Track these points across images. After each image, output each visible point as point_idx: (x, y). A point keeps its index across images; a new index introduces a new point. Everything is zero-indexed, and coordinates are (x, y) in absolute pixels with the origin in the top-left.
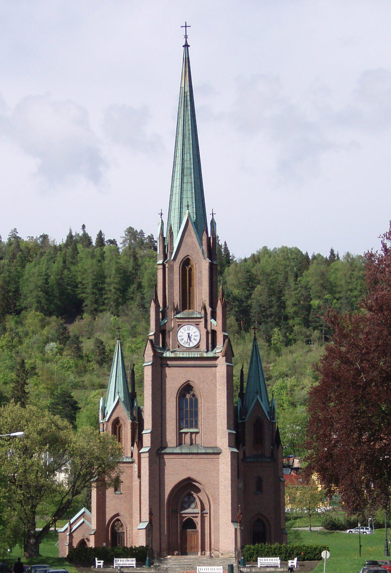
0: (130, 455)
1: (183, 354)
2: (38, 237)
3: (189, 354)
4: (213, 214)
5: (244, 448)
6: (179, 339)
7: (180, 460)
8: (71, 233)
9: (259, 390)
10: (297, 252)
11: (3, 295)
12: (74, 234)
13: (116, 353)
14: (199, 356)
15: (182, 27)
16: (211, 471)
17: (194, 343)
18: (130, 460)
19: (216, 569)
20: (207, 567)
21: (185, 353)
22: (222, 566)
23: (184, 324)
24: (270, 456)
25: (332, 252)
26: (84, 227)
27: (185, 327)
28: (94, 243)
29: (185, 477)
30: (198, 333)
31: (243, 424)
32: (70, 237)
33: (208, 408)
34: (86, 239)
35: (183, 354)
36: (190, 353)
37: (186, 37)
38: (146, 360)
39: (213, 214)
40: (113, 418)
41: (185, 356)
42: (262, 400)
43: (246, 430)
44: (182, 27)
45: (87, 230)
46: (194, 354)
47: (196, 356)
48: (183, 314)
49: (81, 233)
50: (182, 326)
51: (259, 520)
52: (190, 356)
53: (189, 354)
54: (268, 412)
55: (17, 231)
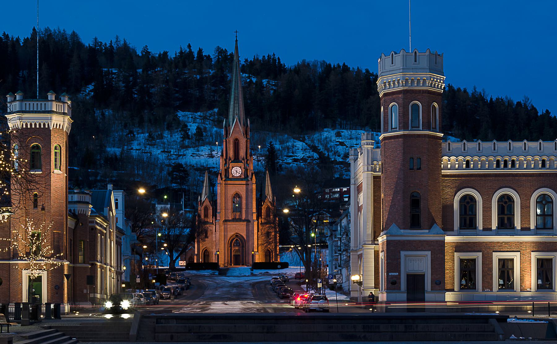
6: (233, 173)
17: (238, 175)
30: (241, 170)
51: (206, 250)
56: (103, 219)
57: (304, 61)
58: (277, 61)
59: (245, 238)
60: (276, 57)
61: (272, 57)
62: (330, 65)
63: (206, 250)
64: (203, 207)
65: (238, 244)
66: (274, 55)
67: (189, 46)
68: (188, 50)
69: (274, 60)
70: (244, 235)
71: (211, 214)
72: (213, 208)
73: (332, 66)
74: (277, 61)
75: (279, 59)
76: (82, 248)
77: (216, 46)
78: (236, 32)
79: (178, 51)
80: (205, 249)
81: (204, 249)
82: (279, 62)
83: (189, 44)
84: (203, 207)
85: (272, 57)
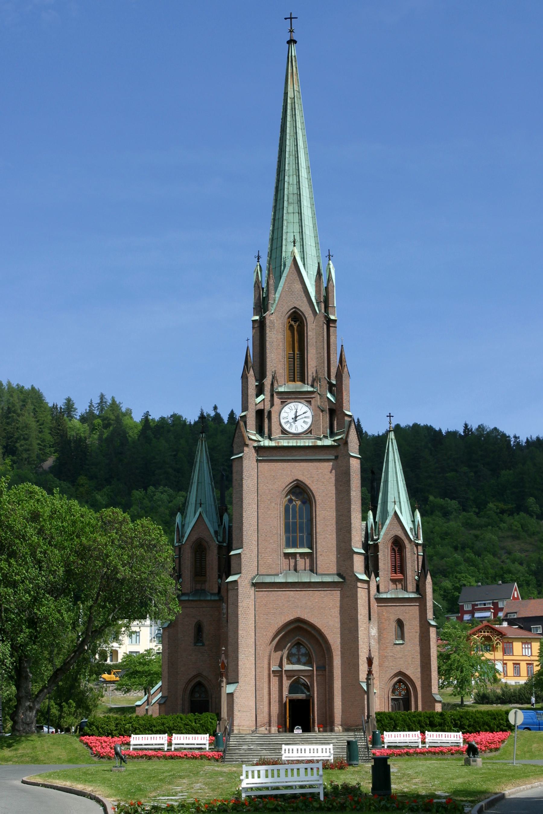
0: (216, 591)
1: (288, 442)
2: (169, 416)
3: (297, 443)
4: (329, 255)
5: (378, 579)
7: (284, 593)
8: (202, 414)
9: (397, 500)
10: (429, 429)
11: (69, 405)
12: (205, 414)
13: (198, 452)
14: (310, 444)
15: (286, 19)
16: (330, 609)
18: (217, 598)
19: (307, 751)
20: (303, 747)
21: (291, 441)
22: (332, 745)
23: (289, 401)
24: (415, 590)
25: (466, 425)
26: (215, 408)
27: (292, 405)
28: (226, 421)
29: (292, 618)
31: (376, 546)
32: (202, 417)
33: (324, 518)
34: (218, 417)
35: (288, 442)
36: (299, 441)
37: (291, 31)
38: (235, 452)
39: (329, 255)
40: (193, 538)
41: (291, 444)
42: (401, 513)
43: (380, 555)
44: (286, 19)
45: (218, 411)
46: (305, 442)
47: (307, 444)
48: (288, 388)
49: (213, 414)
50: (286, 403)
51: (199, 684)
52: (298, 444)
53: (297, 443)
54: (411, 529)
55: (150, 414)
63: (199, 684)
67: (215, 408)
75: (358, 420)
78: (390, 416)
81: (190, 681)
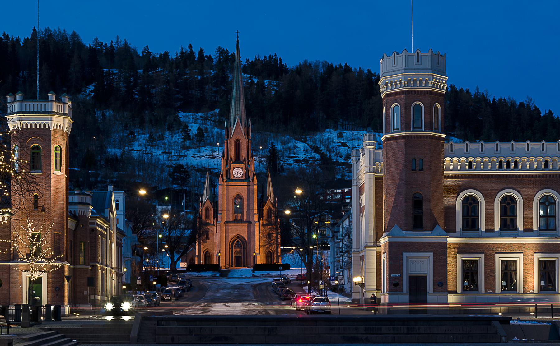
6: (234, 174)
30: (242, 171)
51: (207, 251)
56: (104, 220)
57: (305, 61)
58: (279, 62)
59: (247, 240)
60: (278, 57)
61: (274, 57)
62: (332, 65)
63: (207, 251)
64: (204, 208)
65: (239, 246)
66: (276, 55)
67: (190, 46)
68: (189, 50)
69: (276, 61)
70: (245, 236)
71: (213, 215)
72: (214, 210)
73: (334, 67)
74: (279, 62)
75: (280, 59)
76: (83, 249)
77: (217, 47)
78: (238, 32)
79: (179, 51)
80: (206, 250)
81: (205, 250)
82: (281, 62)
83: (190, 44)
84: (204, 208)
85: (274, 57)
